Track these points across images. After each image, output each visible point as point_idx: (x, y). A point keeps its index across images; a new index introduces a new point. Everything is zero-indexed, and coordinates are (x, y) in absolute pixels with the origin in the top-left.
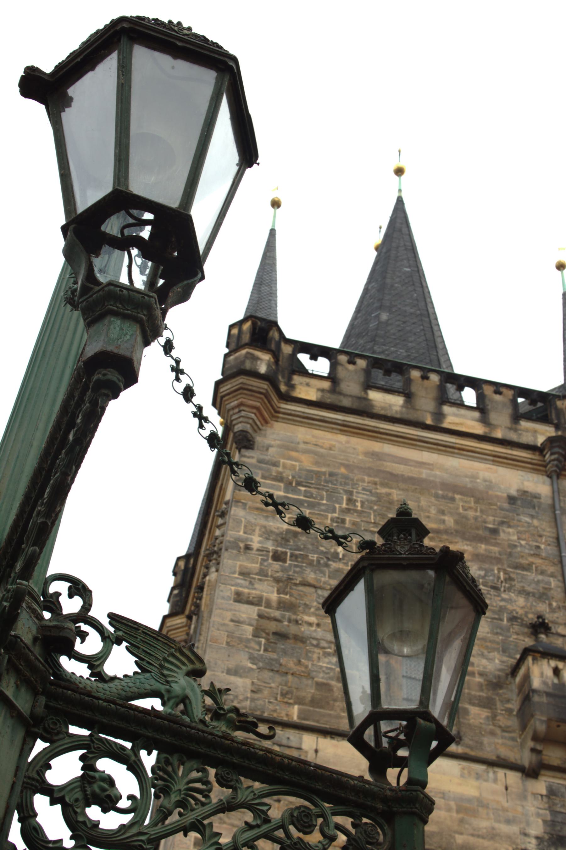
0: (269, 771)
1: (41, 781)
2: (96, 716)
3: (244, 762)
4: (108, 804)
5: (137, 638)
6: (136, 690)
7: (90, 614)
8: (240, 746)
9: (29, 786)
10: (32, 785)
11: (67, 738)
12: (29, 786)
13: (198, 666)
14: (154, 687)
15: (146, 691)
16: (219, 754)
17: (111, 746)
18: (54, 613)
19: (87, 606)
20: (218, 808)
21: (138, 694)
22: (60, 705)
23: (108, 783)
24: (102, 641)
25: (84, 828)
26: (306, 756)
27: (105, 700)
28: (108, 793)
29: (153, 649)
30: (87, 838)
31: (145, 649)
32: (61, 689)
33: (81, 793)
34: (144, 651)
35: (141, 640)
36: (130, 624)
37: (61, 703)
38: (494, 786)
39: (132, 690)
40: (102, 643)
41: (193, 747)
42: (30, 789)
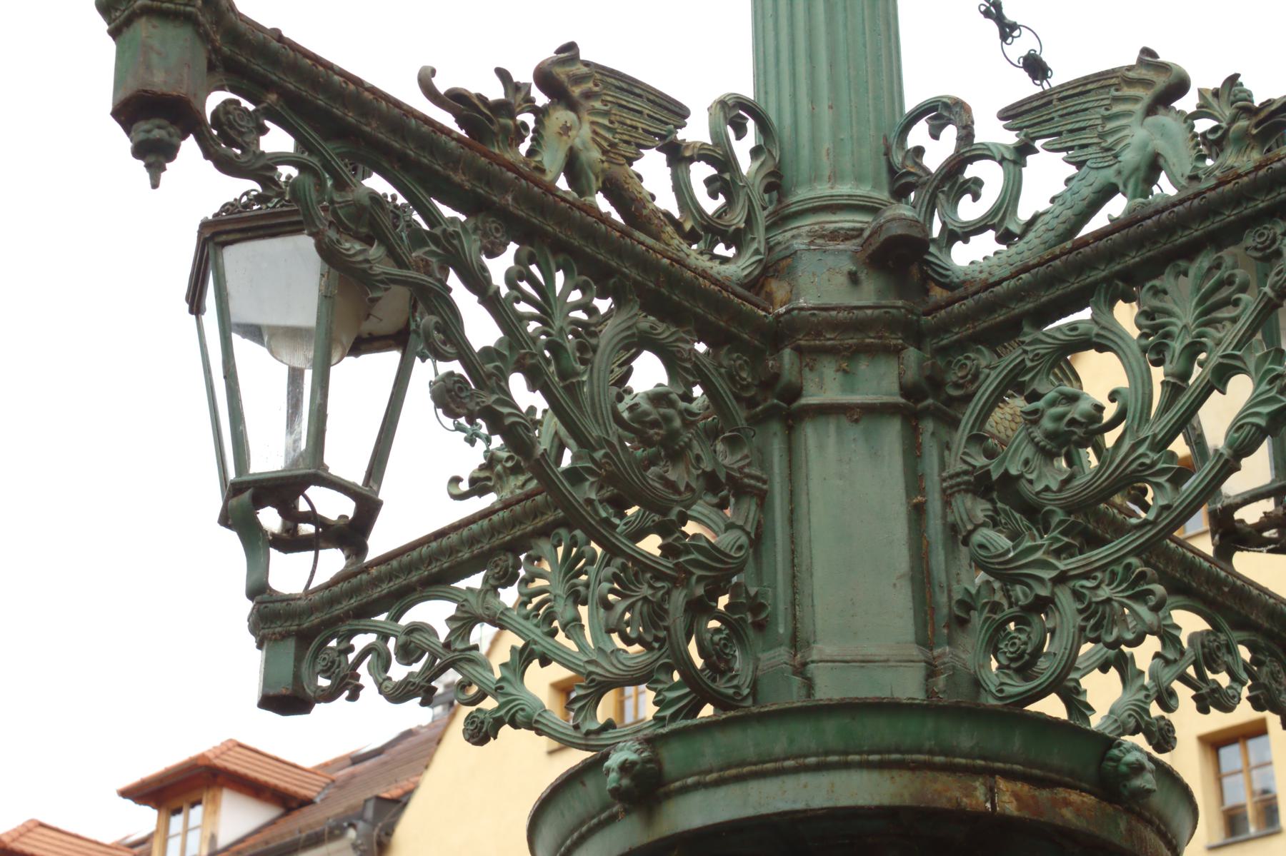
0: (380, 135)
1: (970, 468)
2: (1014, 309)
3: (1279, 194)
4: (1074, 433)
5: (1053, 118)
6: (1069, 213)
7: (976, 141)
8: (182, 8)
9: (955, 489)
10: (959, 484)
11: (992, 372)
12: (955, 489)
13: (1161, 81)
14: (1097, 185)
15: (1086, 202)
16: (1229, 216)
17: (1054, 338)
18: (917, 187)
19: (966, 135)
20: (1259, 308)
21: (1076, 215)
22: (957, 333)
23: (1064, 401)
24: (669, 165)
25: (1050, 496)
26: (1003, 548)
27: (1012, 276)
28: (1069, 417)
29: (1082, 116)
30: (1061, 508)
31: (1070, 127)
32: (943, 311)
33: (1030, 446)
34: (1071, 131)
35: (1061, 116)
36: (1035, 104)
37: (957, 330)
38: (537, 713)
39: (1062, 219)
40: (669, 169)
41: (1181, 238)
42: (959, 491)
